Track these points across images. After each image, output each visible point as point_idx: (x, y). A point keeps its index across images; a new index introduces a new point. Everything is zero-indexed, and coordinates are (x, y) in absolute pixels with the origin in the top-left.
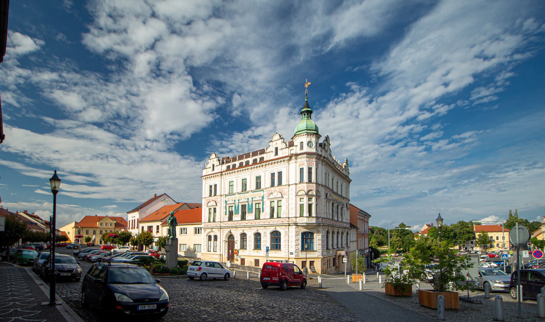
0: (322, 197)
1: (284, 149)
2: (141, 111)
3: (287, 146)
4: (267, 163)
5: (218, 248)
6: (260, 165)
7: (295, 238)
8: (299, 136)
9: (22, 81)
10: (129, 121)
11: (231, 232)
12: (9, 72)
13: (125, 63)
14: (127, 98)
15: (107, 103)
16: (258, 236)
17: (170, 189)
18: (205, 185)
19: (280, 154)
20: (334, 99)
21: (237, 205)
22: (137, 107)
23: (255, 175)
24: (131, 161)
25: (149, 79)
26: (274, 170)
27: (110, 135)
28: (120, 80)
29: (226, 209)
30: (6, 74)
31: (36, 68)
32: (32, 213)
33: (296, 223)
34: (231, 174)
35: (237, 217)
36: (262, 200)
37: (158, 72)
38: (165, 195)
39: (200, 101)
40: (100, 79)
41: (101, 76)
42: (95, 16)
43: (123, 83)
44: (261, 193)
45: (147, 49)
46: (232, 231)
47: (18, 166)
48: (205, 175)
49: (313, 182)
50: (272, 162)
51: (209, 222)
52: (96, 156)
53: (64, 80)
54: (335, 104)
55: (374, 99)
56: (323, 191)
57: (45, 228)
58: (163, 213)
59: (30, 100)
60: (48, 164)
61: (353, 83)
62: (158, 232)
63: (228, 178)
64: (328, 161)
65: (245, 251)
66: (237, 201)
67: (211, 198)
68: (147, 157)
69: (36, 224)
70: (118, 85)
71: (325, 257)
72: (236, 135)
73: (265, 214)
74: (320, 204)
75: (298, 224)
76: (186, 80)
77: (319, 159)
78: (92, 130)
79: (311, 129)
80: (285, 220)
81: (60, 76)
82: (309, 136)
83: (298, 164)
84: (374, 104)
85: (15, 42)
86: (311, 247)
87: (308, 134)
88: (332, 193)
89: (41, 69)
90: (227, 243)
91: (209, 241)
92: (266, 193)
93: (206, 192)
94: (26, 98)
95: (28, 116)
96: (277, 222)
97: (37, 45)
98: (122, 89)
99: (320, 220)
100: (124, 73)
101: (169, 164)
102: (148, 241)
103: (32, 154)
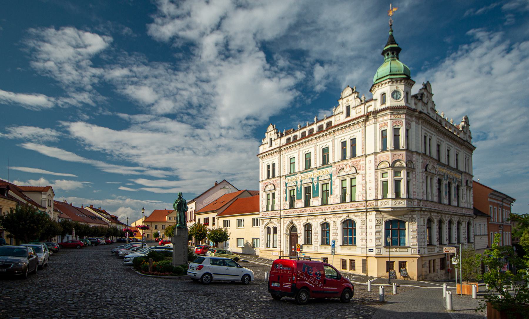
0: (417, 170)
1: (358, 106)
2: (213, 98)
3: (363, 102)
4: (336, 129)
5: (278, 242)
6: (326, 132)
7: (376, 228)
8: (379, 86)
9: (96, 81)
10: (201, 109)
11: (292, 223)
12: (84, 73)
13: (192, 48)
14: (197, 85)
15: (177, 94)
16: (325, 227)
17: (251, 180)
18: (262, 165)
19: (354, 114)
20: (451, 54)
21: (299, 187)
22: (208, 94)
23: (321, 146)
24: (207, 152)
25: (217, 62)
26: (345, 137)
27: (184, 126)
28: (188, 68)
29: (286, 193)
30: (81, 75)
31: (108, 66)
32: (99, 208)
33: (376, 207)
34: (292, 148)
35: (299, 204)
36: (331, 179)
37: (227, 53)
38: (225, 182)
39: (275, 79)
40: (169, 69)
41: (169, 66)
42: (157, 5)
43: (193, 70)
44: (329, 170)
45: (212, 31)
46: (294, 222)
47: (101, 164)
48: (262, 152)
49: (401, 148)
50: (341, 127)
51: (268, 210)
52: (172, 149)
53: (134, 74)
54: (452, 61)
55: (515, 46)
56: (419, 162)
57: (110, 222)
58: (221, 203)
59: (105, 98)
60: (128, 160)
61: (477, 30)
62: (214, 224)
63: (287, 154)
64: (427, 118)
65: (310, 247)
66: (299, 183)
67: (269, 181)
68: (223, 146)
69: (101, 219)
70: (187, 73)
71: (424, 255)
72: (323, 113)
73: (335, 197)
74: (414, 180)
75: (380, 209)
76: (258, 58)
77: (411, 116)
78: (165, 122)
79: (397, 73)
80: (361, 204)
81: (131, 71)
82: (394, 84)
83: (378, 125)
84: (514, 54)
85: (87, 42)
86: (402, 242)
87: (392, 81)
88: (438, 164)
89: (113, 66)
90: (289, 236)
91: (267, 234)
92: (334, 169)
93: (263, 175)
94: (102, 97)
95: (104, 114)
96: (351, 207)
97: (105, 42)
98: (192, 78)
99: (415, 203)
100: (192, 59)
101: (246, 152)
102: (200, 235)
103: (112, 151)
